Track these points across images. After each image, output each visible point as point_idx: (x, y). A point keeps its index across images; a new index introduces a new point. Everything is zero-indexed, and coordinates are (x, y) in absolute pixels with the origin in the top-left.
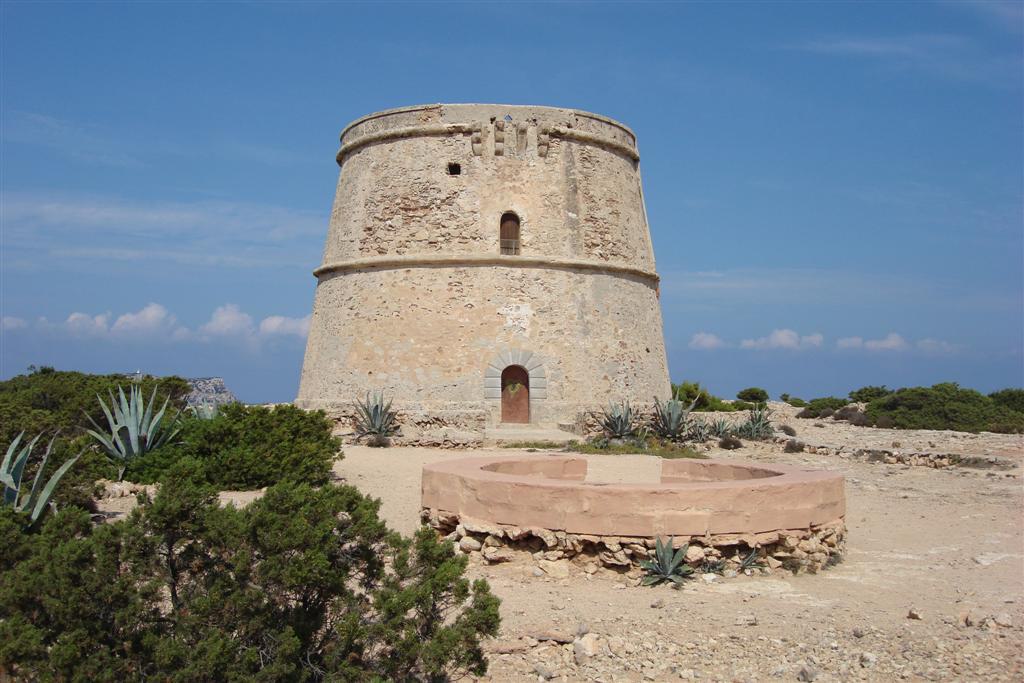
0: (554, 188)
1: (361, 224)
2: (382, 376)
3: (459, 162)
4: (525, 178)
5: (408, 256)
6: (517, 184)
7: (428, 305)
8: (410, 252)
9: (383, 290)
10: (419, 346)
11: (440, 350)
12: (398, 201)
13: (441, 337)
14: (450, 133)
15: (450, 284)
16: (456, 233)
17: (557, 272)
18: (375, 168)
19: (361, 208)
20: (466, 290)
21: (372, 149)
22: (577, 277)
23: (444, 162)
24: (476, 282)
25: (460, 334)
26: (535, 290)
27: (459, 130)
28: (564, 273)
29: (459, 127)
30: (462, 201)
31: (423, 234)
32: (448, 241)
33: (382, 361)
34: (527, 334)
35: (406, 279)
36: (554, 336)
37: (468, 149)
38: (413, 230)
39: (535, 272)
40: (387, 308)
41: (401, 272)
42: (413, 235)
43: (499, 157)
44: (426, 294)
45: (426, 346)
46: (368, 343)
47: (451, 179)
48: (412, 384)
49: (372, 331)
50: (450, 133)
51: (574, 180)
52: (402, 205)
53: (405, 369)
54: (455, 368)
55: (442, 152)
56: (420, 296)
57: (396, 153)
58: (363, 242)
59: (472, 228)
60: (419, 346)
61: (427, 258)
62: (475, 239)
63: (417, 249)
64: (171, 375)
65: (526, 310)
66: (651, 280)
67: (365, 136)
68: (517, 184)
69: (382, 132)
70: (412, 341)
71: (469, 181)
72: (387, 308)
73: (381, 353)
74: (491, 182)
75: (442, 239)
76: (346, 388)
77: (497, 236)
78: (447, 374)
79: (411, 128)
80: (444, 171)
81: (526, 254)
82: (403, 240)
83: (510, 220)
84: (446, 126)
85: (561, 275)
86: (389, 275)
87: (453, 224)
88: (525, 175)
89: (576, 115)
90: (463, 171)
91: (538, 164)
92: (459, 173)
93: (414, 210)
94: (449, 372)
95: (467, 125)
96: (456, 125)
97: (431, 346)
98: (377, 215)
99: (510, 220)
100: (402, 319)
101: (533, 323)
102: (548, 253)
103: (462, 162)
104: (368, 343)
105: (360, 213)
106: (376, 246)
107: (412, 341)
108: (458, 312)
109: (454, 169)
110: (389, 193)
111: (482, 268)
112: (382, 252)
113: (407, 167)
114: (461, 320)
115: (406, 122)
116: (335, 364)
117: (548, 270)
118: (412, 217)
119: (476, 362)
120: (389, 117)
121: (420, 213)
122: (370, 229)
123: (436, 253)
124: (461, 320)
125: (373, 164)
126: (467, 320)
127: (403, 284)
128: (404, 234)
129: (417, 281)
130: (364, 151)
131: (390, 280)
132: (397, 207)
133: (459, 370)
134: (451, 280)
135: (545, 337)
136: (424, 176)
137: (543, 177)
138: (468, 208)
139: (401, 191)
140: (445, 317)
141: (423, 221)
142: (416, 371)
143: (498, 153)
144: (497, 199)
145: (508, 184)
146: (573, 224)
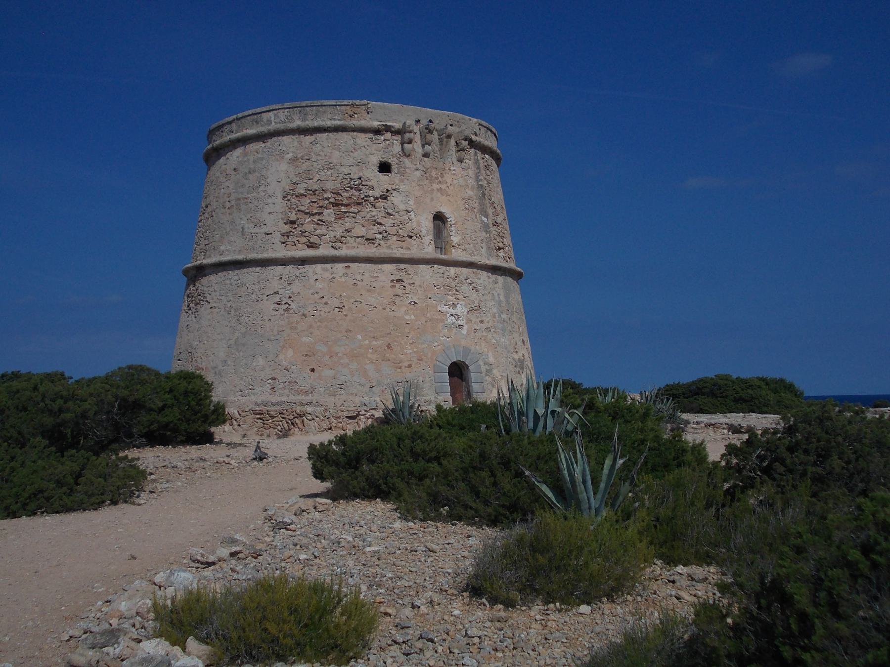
0: (470, 193)
1: (280, 216)
2: (329, 373)
3: (390, 161)
4: (449, 181)
5: (344, 252)
6: (444, 187)
7: (372, 300)
8: (348, 248)
9: (319, 285)
10: (367, 342)
11: (389, 346)
12: (328, 195)
13: (390, 333)
14: (377, 132)
15: (393, 281)
16: (393, 231)
17: (481, 272)
18: (294, 160)
19: (279, 200)
20: (408, 287)
21: (286, 139)
22: (494, 277)
23: (375, 160)
24: (417, 280)
25: (407, 331)
26: (466, 288)
27: (388, 129)
28: (485, 273)
29: (390, 126)
30: (396, 199)
31: (360, 231)
32: (385, 238)
33: (327, 358)
34: (464, 332)
35: (346, 275)
36: (484, 334)
37: (397, 148)
38: (348, 225)
39: (465, 271)
40: (326, 303)
41: (340, 267)
42: (348, 231)
43: (425, 159)
44: (369, 291)
45: (374, 343)
46: (305, 339)
47: (383, 177)
48: (363, 381)
49: (311, 326)
50: (377, 132)
51: (482, 186)
52: (332, 200)
53: (354, 366)
54: (406, 364)
55: (374, 151)
56: (364, 292)
57: (318, 148)
58: (287, 235)
59: (409, 227)
60: (367, 342)
61: (371, 255)
62: (411, 237)
63: (355, 244)
64: (788, 379)
65: (460, 309)
66: (516, 276)
67: (273, 127)
68: (444, 187)
69: (297, 123)
70: (359, 337)
71: (402, 181)
72: (326, 303)
73: (324, 349)
74: (421, 183)
75: (379, 236)
76: (282, 385)
77: (431, 237)
78: (399, 370)
79: (338, 123)
80: (376, 169)
81: (457, 254)
82: (338, 234)
83: (439, 218)
84: (376, 124)
85: (484, 274)
86: (326, 270)
87: (388, 222)
88: (448, 178)
89: (480, 124)
90: (394, 167)
91: (457, 168)
92: (390, 172)
93: (346, 205)
94: (400, 368)
95: (397, 125)
96: (389, 124)
97: (379, 342)
98: (302, 208)
99: (439, 218)
100: (346, 315)
101: (469, 321)
102: (472, 254)
103: (393, 162)
104: (305, 339)
105: (279, 205)
106: (304, 240)
107: (359, 337)
108: (403, 309)
109: (385, 168)
110: (315, 187)
111: (421, 266)
112: (311, 246)
113: (335, 161)
114: (407, 317)
115: (329, 116)
116: (261, 362)
117: (475, 270)
118: (345, 212)
119: (424, 358)
120: (308, 109)
121: (353, 209)
122: (293, 222)
123: (375, 250)
124: (407, 317)
125: (290, 155)
126: (413, 317)
127: (343, 279)
128: (338, 231)
129: (359, 277)
130: (270, 142)
131: (327, 275)
132: (327, 202)
133: (410, 366)
134: (393, 277)
135: (478, 334)
136: (355, 173)
137: (461, 181)
138: (402, 207)
139: (330, 185)
140: (391, 313)
141: (358, 217)
142: (367, 367)
143: (426, 155)
144: (428, 200)
145: (435, 186)
146: (485, 227)
